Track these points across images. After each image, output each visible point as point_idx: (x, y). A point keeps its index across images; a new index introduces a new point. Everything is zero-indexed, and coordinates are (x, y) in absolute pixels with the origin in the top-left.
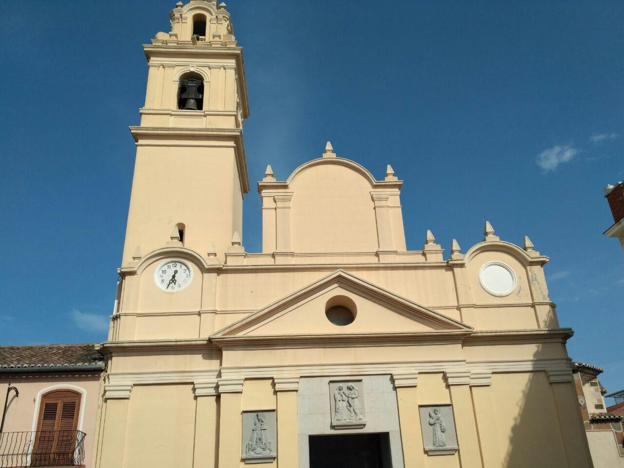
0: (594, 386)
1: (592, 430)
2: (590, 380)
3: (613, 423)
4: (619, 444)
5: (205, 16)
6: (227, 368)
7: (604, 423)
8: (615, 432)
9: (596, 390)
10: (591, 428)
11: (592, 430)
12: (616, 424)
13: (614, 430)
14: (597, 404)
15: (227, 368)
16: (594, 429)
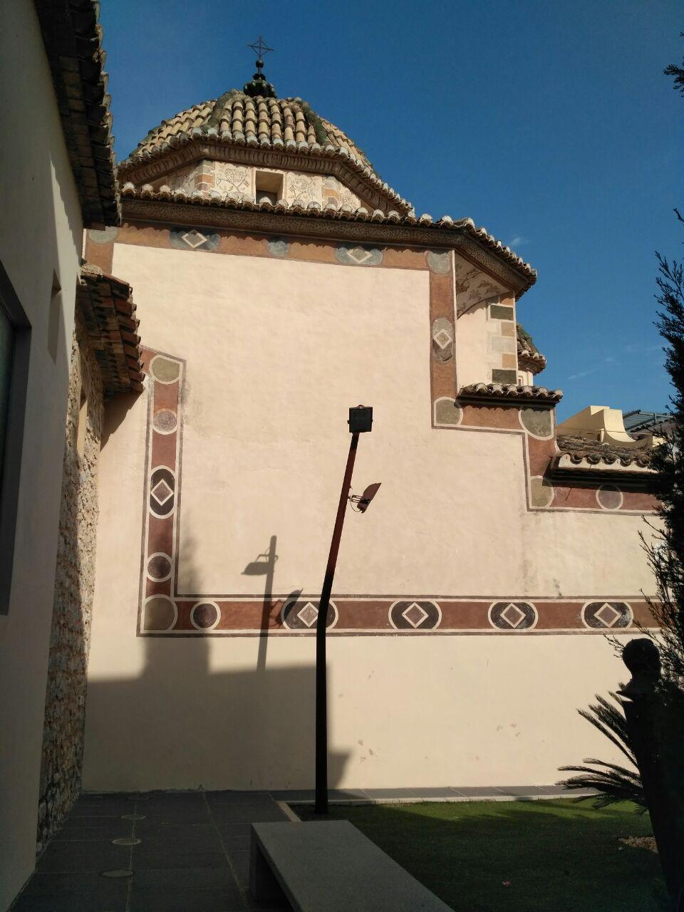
0: (504, 317)
1: (459, 425)
2: (494, 299)
3: (530, 411)
4: (534, 473)
5: (291, 628)
6: (558, 616)
7: (499, 410)
8: (530, 438)
9: (505, 331)
10: (456, 419)
11: (459, 425)
12: (536, 416)
13: (526, 431)
14: (500, 367)
15: (558, 616)
16: (463, 423)
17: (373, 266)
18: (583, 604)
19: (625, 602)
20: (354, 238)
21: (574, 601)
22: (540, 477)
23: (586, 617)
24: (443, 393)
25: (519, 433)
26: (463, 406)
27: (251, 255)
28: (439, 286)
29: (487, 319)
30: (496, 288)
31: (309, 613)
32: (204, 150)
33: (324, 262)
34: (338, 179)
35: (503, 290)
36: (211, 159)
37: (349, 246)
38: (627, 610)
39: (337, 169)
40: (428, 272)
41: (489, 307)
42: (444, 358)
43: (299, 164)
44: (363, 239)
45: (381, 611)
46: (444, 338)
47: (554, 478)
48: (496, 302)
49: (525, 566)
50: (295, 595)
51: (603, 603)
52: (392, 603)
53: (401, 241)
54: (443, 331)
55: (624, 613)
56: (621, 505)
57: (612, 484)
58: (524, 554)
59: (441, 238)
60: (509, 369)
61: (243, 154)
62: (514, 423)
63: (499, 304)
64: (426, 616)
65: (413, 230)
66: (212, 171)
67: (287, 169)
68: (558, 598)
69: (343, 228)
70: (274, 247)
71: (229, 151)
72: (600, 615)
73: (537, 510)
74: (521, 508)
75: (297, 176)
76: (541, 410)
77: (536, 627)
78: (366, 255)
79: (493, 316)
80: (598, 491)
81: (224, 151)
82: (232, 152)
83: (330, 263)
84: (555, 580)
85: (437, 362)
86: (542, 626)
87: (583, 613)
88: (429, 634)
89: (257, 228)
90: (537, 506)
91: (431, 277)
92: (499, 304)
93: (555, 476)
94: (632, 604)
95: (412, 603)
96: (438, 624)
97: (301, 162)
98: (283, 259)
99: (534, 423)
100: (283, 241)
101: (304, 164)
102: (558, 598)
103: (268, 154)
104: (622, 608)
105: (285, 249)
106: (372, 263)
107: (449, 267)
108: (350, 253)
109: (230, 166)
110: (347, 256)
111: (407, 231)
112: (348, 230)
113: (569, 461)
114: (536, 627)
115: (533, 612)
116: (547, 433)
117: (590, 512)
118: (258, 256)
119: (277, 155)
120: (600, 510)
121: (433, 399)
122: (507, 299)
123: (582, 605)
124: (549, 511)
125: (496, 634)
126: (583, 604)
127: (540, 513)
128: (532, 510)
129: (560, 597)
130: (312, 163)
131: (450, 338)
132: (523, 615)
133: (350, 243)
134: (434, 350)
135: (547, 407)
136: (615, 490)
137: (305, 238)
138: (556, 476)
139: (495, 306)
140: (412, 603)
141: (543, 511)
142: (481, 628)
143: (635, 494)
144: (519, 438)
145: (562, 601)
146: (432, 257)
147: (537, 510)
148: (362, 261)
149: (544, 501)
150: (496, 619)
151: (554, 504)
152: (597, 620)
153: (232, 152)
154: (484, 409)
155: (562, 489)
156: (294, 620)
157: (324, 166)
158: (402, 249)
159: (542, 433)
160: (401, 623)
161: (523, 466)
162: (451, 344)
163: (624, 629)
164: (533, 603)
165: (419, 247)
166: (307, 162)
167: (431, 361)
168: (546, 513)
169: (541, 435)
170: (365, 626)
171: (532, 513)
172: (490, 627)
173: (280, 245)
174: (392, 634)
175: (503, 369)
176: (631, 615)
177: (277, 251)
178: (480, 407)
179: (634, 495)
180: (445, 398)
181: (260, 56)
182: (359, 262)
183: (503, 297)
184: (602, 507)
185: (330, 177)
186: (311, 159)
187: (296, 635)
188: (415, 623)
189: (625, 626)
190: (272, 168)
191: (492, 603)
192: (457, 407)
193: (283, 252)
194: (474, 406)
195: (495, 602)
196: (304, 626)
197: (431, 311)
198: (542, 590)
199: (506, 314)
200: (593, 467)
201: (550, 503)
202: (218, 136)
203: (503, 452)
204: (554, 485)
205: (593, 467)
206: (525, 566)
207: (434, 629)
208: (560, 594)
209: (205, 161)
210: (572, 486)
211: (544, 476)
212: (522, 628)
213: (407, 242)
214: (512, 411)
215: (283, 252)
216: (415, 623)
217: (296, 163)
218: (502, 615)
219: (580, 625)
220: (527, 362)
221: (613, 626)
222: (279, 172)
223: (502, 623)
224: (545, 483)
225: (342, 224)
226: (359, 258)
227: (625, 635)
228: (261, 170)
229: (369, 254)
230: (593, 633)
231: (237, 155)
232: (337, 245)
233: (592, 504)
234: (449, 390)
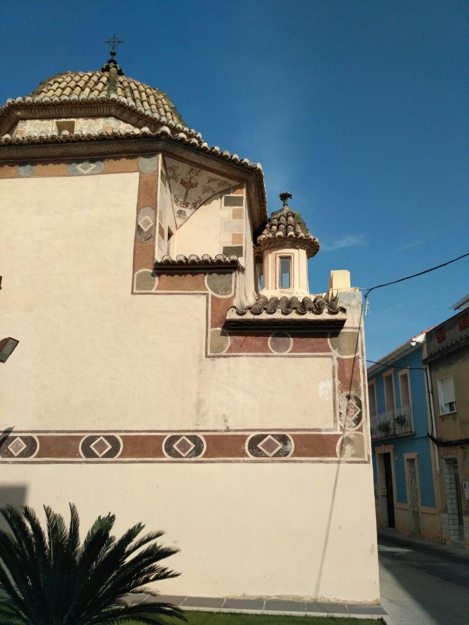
2: (227, 191)
3: (214, 275)
4: (214, 325)
7: (189, 276)
9: (236, 215)
13: (210, 292)
17: (96, 174)
18: (248, 436)
19: (287, 434)
20: (81, 155)
21: (240, 433)
22: (219, 329)
23: (249, 448)
24: (143, 266)
25: (204, 294)
26: (159, 275)
27: (6, 178)
28: (146, 184)
29: (221, 207)
30: (225, 182)
31: (17, 446)
32: (18, 113)
33: (59, 176)
34: (117, 118)
35: (234, 183)
36: (24, 119)
37: (78, 161)
38: (288, 442)
39: (113, 111)
40: (138, 173)
41: (223, 198)
42: (145, 238)
43: (85, 112)
44: (89, 155)
45: (73, 443)
46: (147, 223)
47: (232, 329)
48: (229, 193)
49: (199, 404)
50: (8, 431)
51: (267, 435)
52: (83, 437)
53: (117, 153)
54: (147, 217)
55: (285, 444)
56: (290, 349)
57: (284, 332)
58: (199, 393)
59: (146, 146)
60: (237, 245)
61: (44, 112)
62: (201, 286)
63: (231, 195)
64: (110, 447)
65: (123, 143)
66: (24, 127)
67: (77, 117)
68: (226, 431)
69: (69, 148)
70: (22, 170)
71: (55, 110)
72: (278, 446)
73: (214, 357)
74: (200, 355)
75: (85, 121)
76: (225, 273)
77: (204, 457)
78: (91, 166)
79: (226, 205)
80: (270, 338)
81: (31, 111)
82: (37, 111)
83: (63, 176)
84: (224, 416)
85: (140, 242)
86: (209, 455)
87: (247, 444)
88: (111, 462)
89: (12, 158)
90: (214, 353)
91: (140, 177)
92: (231, 195)
93: (232, 328)
94: (294, 436)
95: (99, 437)
96: (119, 454)
97: (86, 110)
98: (28, 177)
99: (217, 285)
100: (30, 164)
101: (89, 111)
102: (226, 431)
103: (62, 108)
104: (284, 439)
105: (31, 170)
106: (95, 172)
107: (156, 167)
108: (79, 167)
109: (38, 121)
110: (77, 169)
111: (119, 144)
112: (74, 149)
113: (235, 314)
114: (204, 457)
115: (202, 443)
116: (228, 292)
117: (261, 356)
118: (11, 178)
119: (68, 108)
120: (270, 354)
121: (134, 271)
122: (239, 190)
123: (246, 437)
124: (225, 357)
125: (168, 462)
126: (248, 436)
127: (216, 359)
128: (210, 357)
129: (228, 430)
130: (94, 109)
131: (151, 222)
132: (193, 446)
133: (79, 159)
134: (138, 233)
135: (230, 271)
136: (286, 336)
137: (45, 160)
138: (231, 327)
139: (228, 197)
140: (99, 437)
141: (219, 357)
142: (156, 457)
143: (304, 339)
144: (204, 298)
145: (229, 433)
146: (142, 161)
147: (214, 357)
148: (88, 171)
149: (221, 348)
150: (169, 450)
151: (230, 350)
152: (260, 450)
153: (37, 111)
154: (177, 276)
155: (237, 338)
156: (5, 451)
157: (104, 110)
158: (119, 158)
159: (224, 292)
160: (89, 453)
161: (205, 321)
162: (152, 227)
163: (284, 458)
164: (203, 435)
165: (132, 155)
166: (85, 110)
167: (135, 242)
168: (222, 359)
169: (222, 294)
170: (59, 456)
171: (209, 359)
172: (163, 456)
173: (28, 167)
174: (80, 462)
175: (233, 246)
176: (292, 446)
177: (25, 172)
178: (172, 275)
179: (304, 340)
180: (144, 270)
181: (113, 48)
182: (85, 172)
183: (235, 188)
184: (273, 351)
185: (110, 118)
186: (93, 107)
187: (6, 462)
188: (100, 453)
189: (286, 455)
190: (66, 117)
191: (166, 436)
192: (154, 277)
193: (29, 173)
194: (168, 274)
195: (169, 435)
196: (12, 456)
197: (138, 203)
198: (212, 422)
199: (237, 202)
200: (256, 317)
201: (226, 350)
202: (51, 102)
203: (188, 311)
204: (230, 335)
205: (256, 317)
206: (199, 404)
207: (116, 458)
208: (228, 428)
209: (20, 121)
210: (246, 336)
211: (223, 328)
212: (191, 457)
213: (122, 152)
214: (199, 277)
215: (29, 173)
216: (101, 453)
217: (82, 111)
218: (175, 446)
219: (244, 454)
220: (295, 242)
221: (274, 456)
222: (72, 120)
223: (174, 453)
224: (223, 334)
225: (68, 145)
226: (85, 169)
227: (320, 464)
228: (59, 120)
229: (93, 166)
230: (255, 462)
231: (41, 113)
232: (69, 162)
233: (264, 349)
234: (148, 263)
